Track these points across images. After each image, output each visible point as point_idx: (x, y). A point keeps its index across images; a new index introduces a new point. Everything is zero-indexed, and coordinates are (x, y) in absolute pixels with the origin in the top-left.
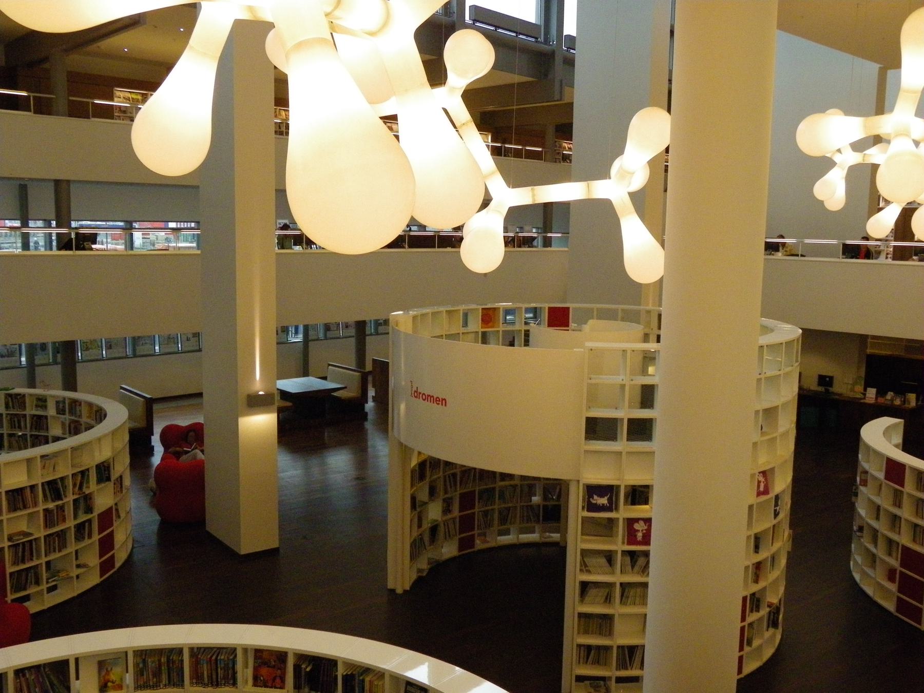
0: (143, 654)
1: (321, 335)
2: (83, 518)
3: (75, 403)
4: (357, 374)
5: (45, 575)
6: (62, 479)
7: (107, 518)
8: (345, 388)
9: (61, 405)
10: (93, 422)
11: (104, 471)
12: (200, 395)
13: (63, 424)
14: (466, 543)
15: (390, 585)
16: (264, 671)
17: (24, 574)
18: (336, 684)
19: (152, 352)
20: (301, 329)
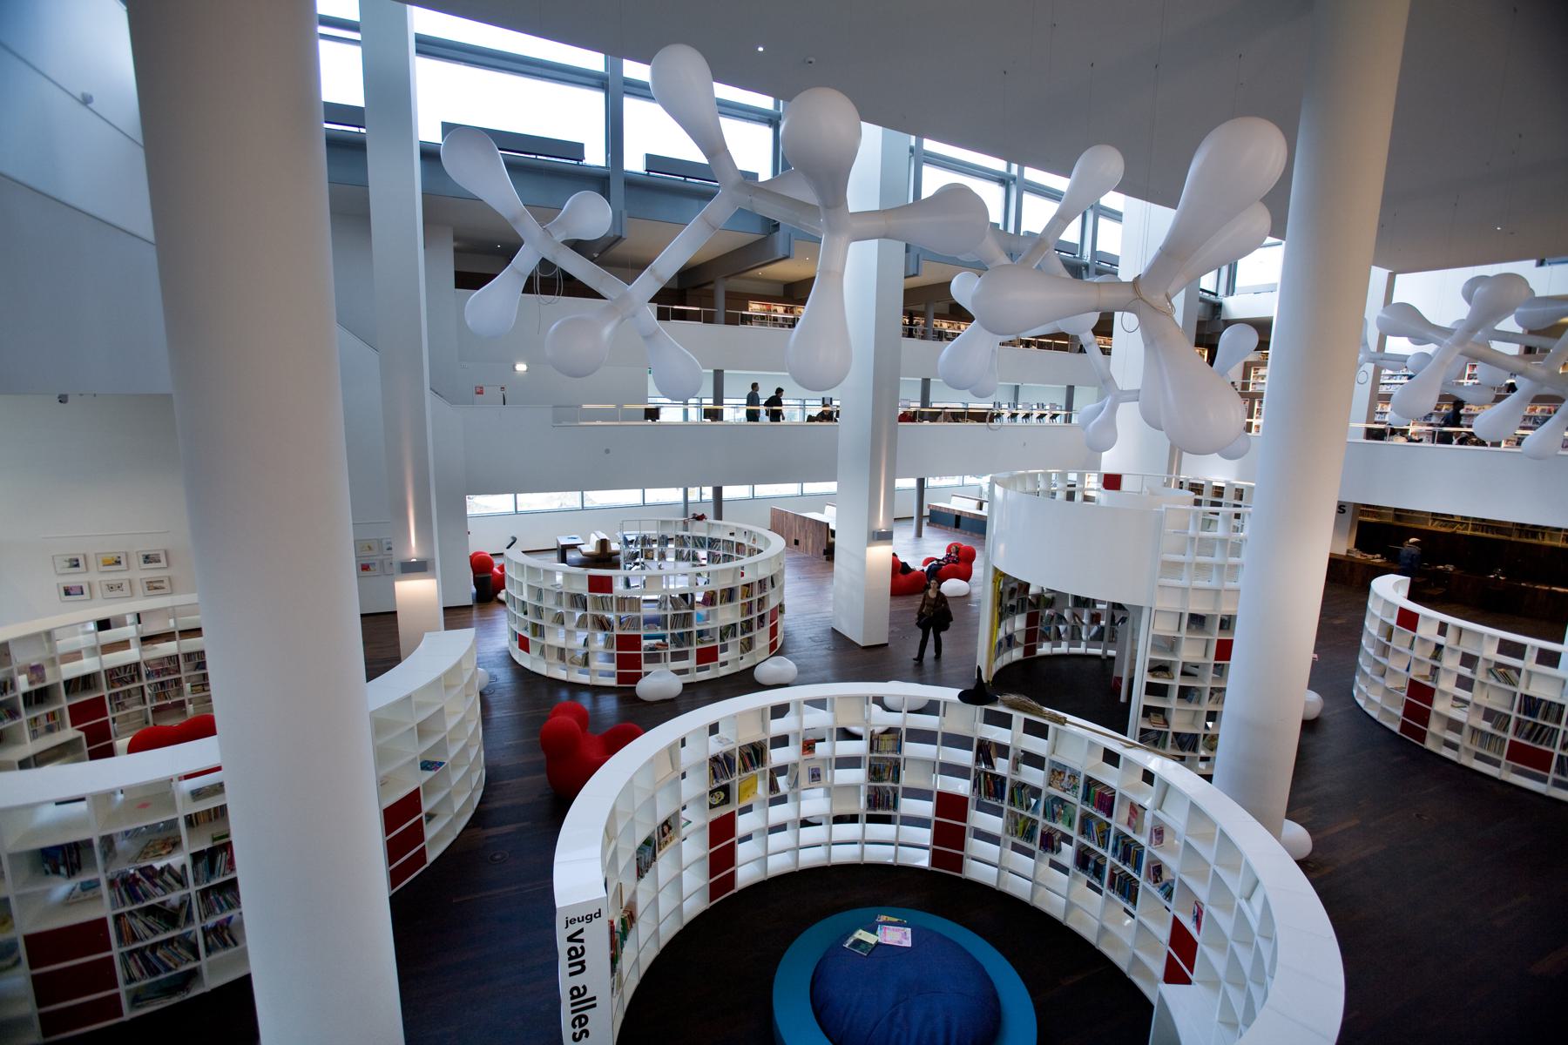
14: (1029, 650)
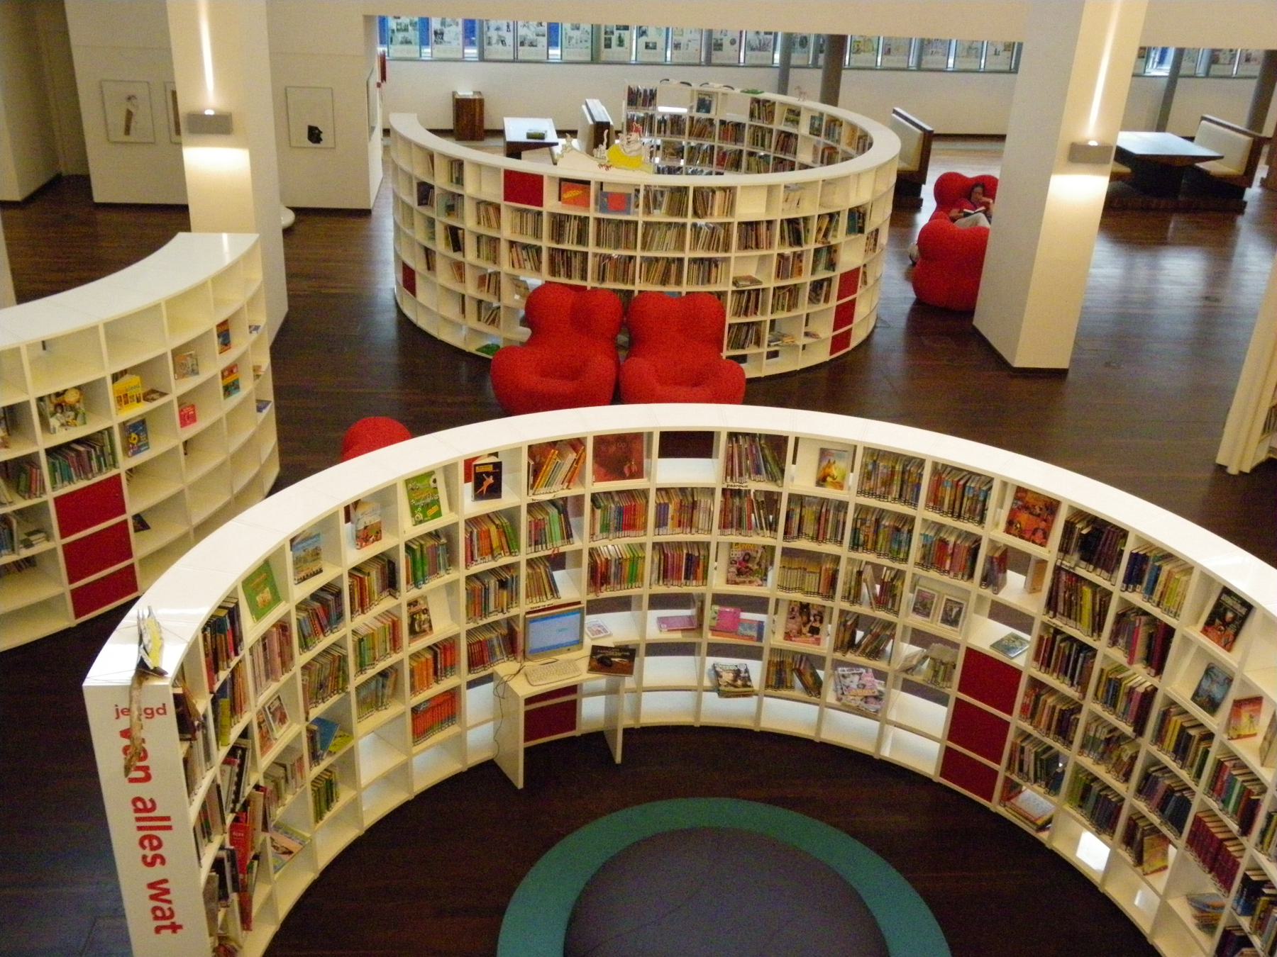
0: (876, 455)
1: (1201, 70)
2: (822, 274)
3: (834, 122)
4: (1247, 138)
5: (767, 336)
6: (806, 219)
7: (851, 281)
8: (1221, 158)
9: (817, 123)
11: (857, 218)
13: (815, 149)
15: (1220, 460)
16: (1024, 517)
17: (745, 329)
18: (1119, 561)
19: (943, 66)
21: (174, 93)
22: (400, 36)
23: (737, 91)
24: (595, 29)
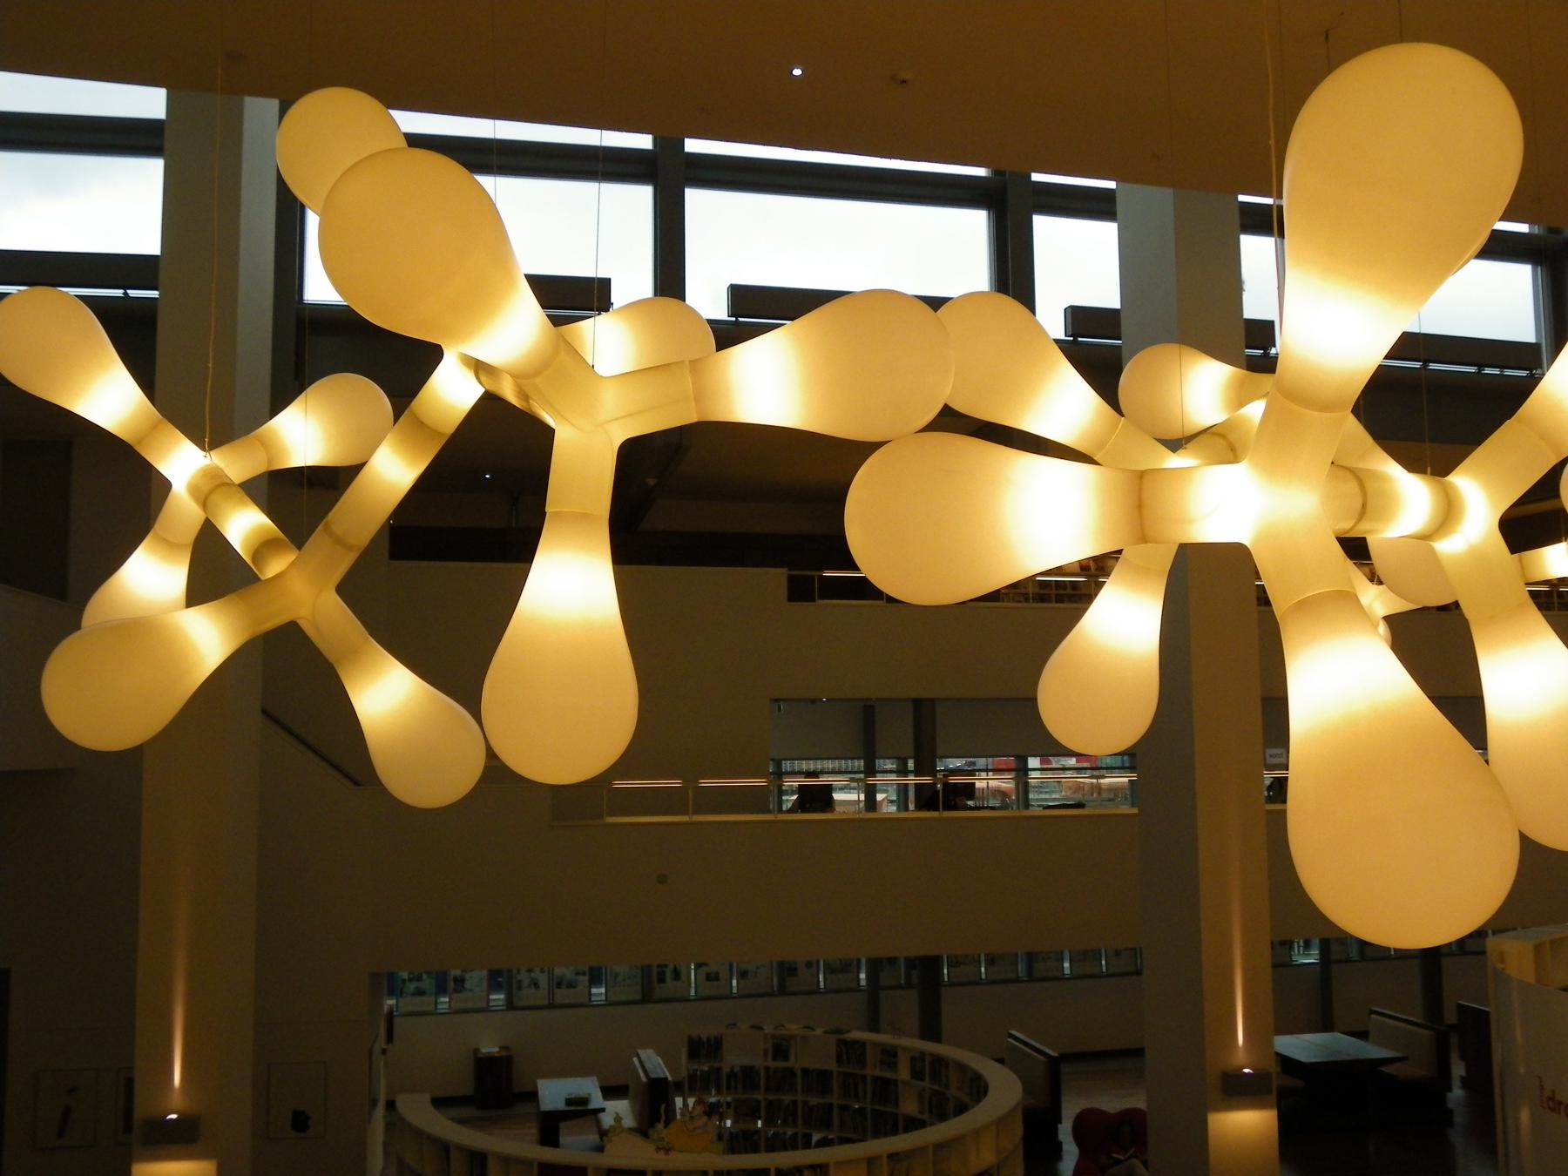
3: (939, 1062)
4: (1426, 1032)
10: (965, 1098)
12: (1139, 1053)
20: (1316, 942)
21: (130, 1083)
22: (412, 987)
23: (819, 1031)
24: (646, 971)
